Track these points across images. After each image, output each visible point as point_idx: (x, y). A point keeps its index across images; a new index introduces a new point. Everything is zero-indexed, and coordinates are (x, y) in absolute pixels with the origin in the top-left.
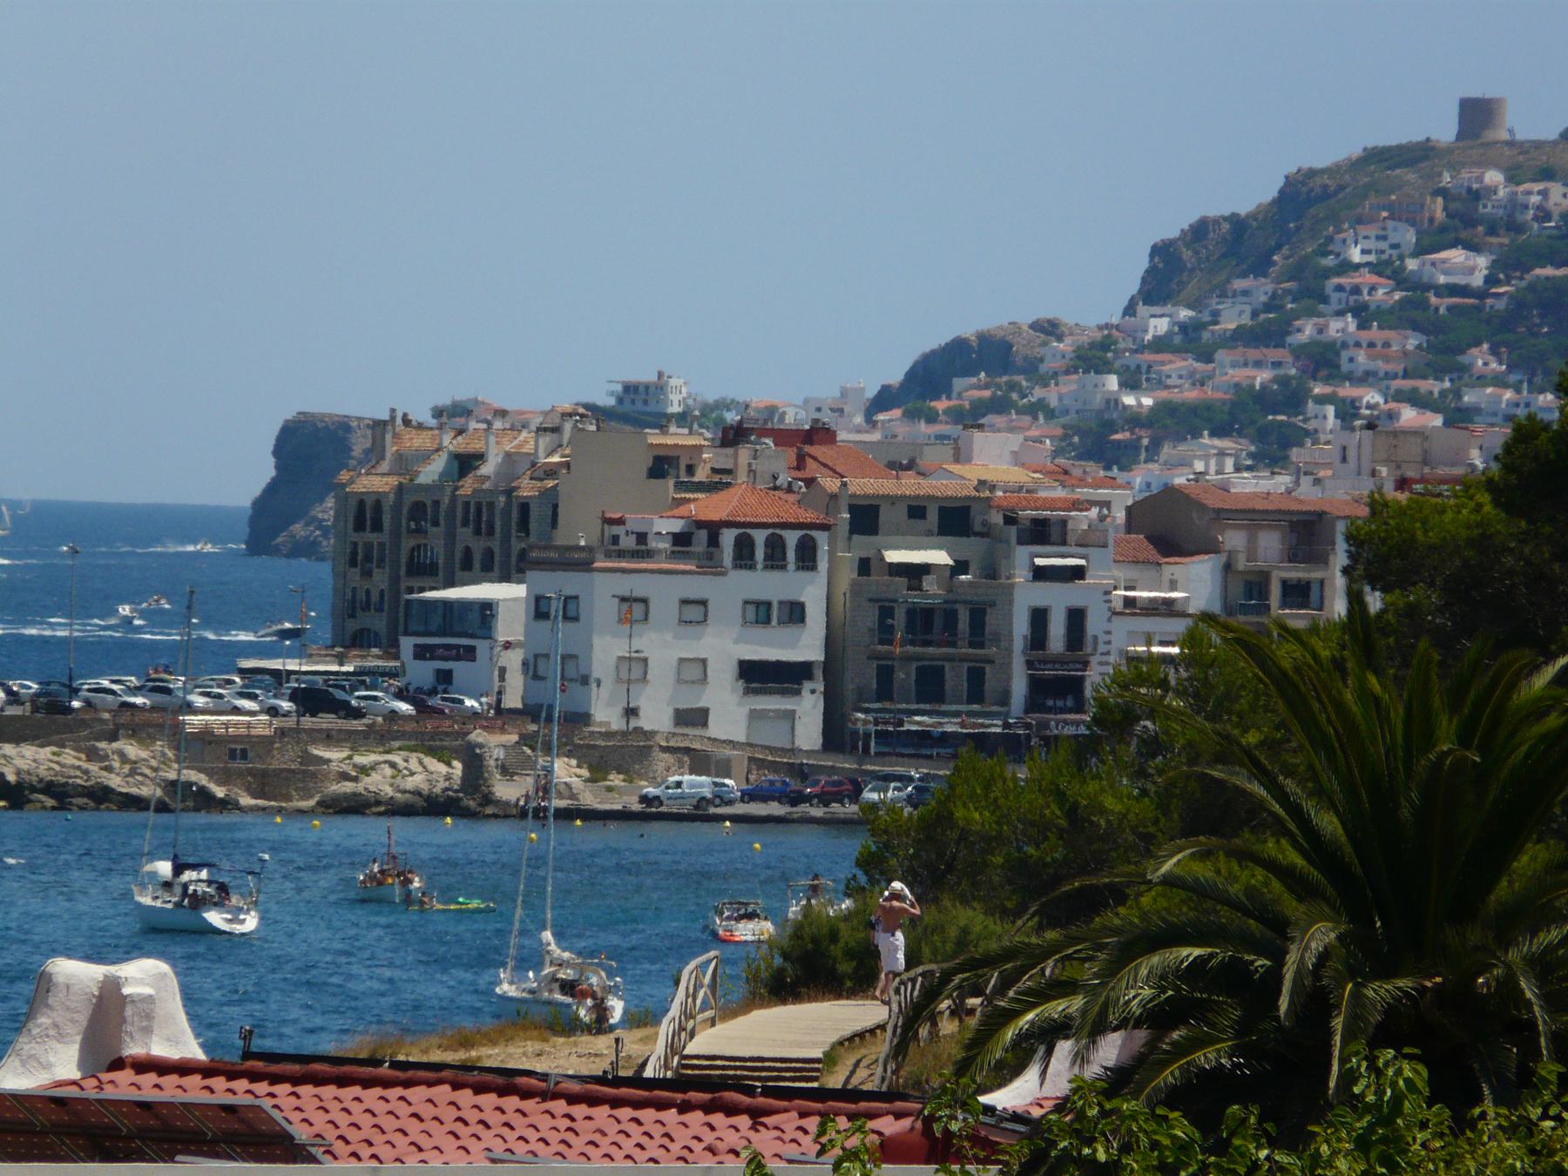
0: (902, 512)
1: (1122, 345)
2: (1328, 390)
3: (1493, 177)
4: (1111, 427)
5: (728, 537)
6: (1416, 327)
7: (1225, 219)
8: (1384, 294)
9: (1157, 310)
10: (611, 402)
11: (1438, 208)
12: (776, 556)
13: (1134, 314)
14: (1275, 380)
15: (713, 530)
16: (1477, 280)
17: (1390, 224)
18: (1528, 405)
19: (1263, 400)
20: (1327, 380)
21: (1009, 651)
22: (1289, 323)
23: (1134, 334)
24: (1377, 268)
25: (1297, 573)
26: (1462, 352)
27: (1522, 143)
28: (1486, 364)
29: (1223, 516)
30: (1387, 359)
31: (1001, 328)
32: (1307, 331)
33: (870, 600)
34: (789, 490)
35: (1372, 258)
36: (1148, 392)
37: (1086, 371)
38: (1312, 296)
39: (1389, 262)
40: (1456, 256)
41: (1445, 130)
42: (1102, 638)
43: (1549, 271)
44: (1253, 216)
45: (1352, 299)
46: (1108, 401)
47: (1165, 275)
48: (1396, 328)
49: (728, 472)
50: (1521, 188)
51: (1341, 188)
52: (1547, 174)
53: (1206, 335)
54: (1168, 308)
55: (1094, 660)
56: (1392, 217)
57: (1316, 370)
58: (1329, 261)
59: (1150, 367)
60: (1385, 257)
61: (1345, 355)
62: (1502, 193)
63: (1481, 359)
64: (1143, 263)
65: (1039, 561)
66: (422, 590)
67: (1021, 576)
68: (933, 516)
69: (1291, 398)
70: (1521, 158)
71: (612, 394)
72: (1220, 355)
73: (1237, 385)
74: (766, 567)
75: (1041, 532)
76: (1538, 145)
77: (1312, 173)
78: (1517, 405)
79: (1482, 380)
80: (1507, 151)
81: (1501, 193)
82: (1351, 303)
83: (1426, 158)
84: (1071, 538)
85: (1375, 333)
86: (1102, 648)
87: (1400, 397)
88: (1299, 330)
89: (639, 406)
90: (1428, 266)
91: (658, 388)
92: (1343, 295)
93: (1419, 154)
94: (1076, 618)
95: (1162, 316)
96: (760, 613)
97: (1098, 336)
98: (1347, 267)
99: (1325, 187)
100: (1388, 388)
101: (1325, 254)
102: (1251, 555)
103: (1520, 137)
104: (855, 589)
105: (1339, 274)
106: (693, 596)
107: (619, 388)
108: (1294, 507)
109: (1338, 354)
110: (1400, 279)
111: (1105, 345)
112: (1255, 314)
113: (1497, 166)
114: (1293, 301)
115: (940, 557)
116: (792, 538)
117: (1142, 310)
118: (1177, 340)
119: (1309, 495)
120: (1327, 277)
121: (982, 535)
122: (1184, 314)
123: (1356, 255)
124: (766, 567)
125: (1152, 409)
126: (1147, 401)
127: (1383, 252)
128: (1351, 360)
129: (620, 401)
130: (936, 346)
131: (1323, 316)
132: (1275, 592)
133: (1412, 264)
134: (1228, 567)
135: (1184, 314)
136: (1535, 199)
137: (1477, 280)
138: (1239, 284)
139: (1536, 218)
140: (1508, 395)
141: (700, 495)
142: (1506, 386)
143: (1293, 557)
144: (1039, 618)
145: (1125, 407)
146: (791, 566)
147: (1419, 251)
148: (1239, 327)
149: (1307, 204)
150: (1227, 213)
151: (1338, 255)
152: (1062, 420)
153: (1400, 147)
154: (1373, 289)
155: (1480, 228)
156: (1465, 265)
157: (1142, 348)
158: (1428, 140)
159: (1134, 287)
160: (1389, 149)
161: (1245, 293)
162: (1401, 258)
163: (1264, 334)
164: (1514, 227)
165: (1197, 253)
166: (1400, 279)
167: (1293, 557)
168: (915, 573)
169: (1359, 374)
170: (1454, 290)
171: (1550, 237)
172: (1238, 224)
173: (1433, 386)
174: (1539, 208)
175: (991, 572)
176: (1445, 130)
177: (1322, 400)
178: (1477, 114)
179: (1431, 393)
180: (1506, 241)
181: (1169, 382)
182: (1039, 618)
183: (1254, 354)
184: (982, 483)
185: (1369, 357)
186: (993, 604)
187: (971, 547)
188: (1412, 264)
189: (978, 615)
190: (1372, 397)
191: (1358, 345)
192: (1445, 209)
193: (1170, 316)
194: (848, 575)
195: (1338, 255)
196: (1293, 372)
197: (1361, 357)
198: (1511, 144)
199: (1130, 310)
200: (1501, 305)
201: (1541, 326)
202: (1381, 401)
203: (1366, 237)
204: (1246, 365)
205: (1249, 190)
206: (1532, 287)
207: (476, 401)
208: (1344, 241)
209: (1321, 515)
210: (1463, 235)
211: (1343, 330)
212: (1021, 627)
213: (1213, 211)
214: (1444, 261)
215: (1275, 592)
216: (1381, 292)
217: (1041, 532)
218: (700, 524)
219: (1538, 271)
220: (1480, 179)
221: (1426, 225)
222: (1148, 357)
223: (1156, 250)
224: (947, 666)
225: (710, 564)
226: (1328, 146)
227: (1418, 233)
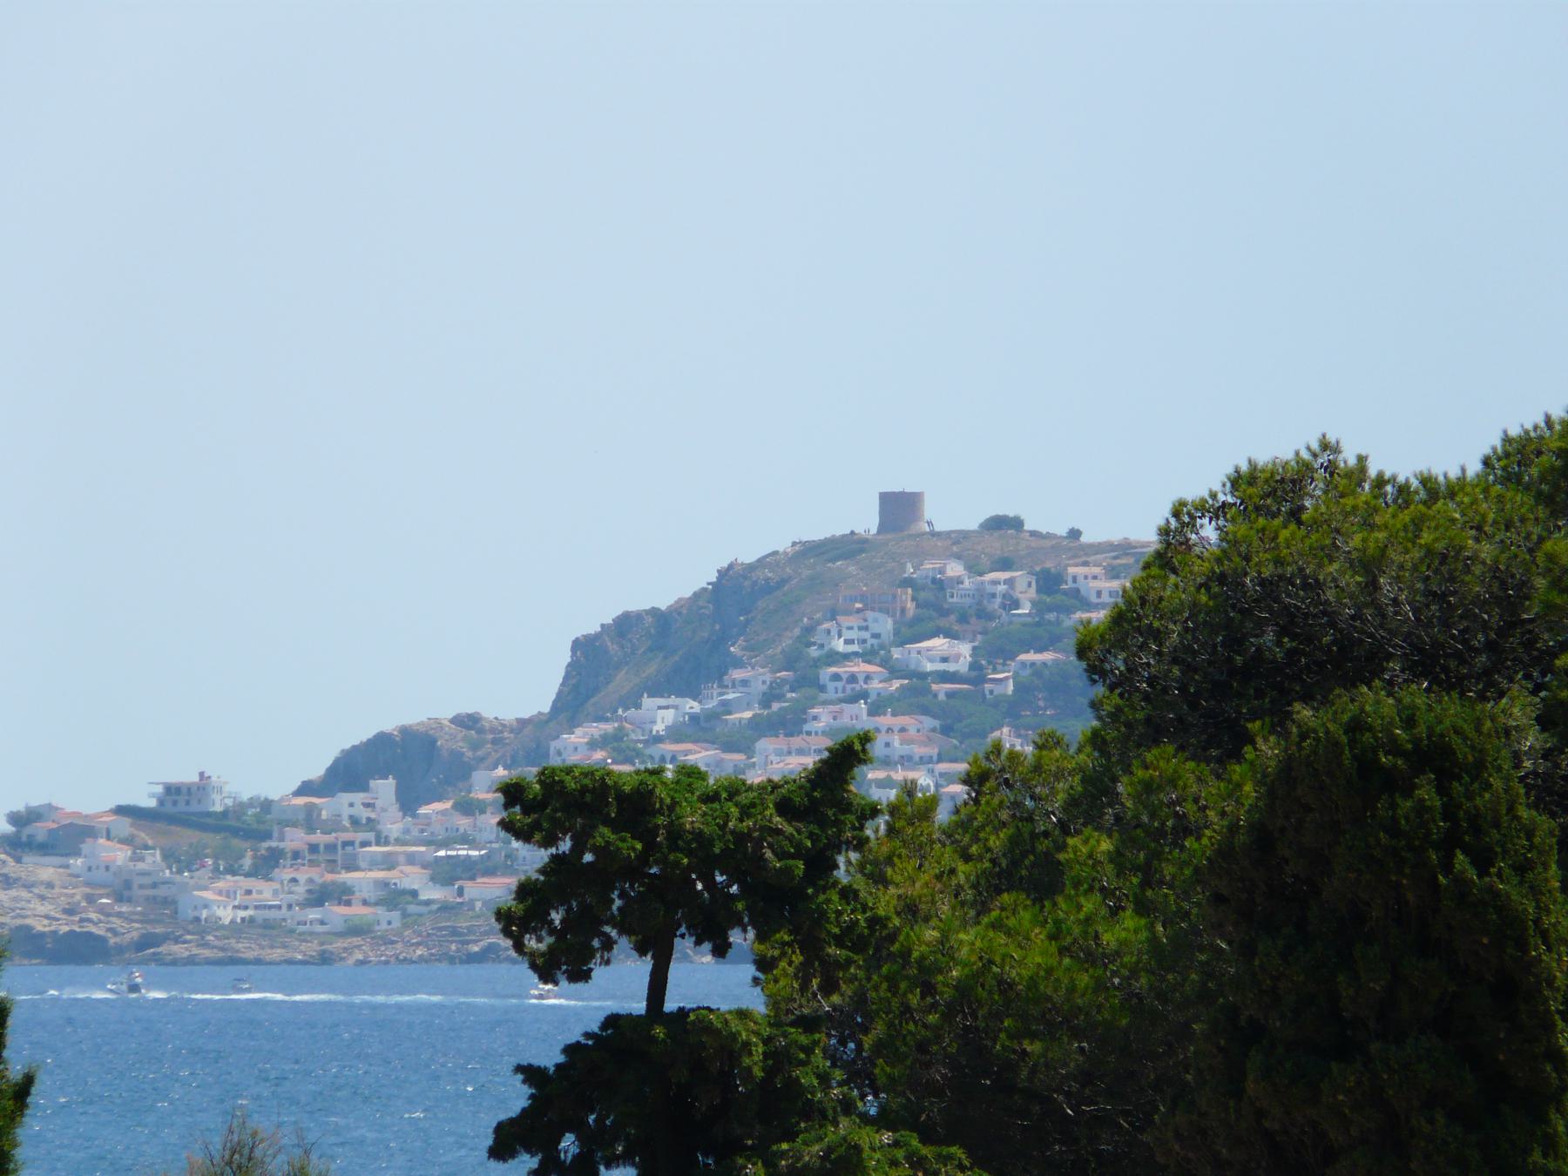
3: (955, 569)
6: (925, 711)
10: (152, 803)
11: (907, 597)
16: (962, 666)
17: (870, 615)
22: (804, 712)
24: (868, 656)
31: (422, 723)
35: (855, 648)
40: (939, 643)
41: (867, 521)
44: (678, 608)
45: (849, 687)
51: (783, 582)
54: (673, 700)
60: (868, 645)
64: (566, 658)
71: (152, 795)
81: (967, 583)
82: (848, 691)
83: (862, 551)
88: (815, 718)
89: (181, 807)
90: (914, 655)
91: (202, 787)
92: (840, 685)
93: (848, 547)
95: (667, 707)
98: (834, 658)
99: (767, 580)
103: (938, 528)
107: (159, 789)
110: (894, 671)
123: (840, 646)
127: (864, 641)
128: (887, 745)
129: (161, 802)
130: (357, 743)
133: (896, 653)
136: (1002, 588)
137: (962, 666)
139: (1003, 606)
151: (822, 646)
154: (868, 678)
158: (852, 533)
161: (745, 683)
164: (984, 615)
165: (622, 647)
170: (945, 677)
171: (1024, 625)
176: (867, 521)
178: (899, 508)
188: (896, 653)
191: (889, 730)
192: (913, 599)
193: (676, 707)
195: (822, 646)
197: (896, 741)
201: (1045, 709)
203: (850, 628)
204: (789, 753)
205: (670, 579)
207: (50, 807)
208: (829, 632)
219: (1023, 657)
220: (942, 571)
223: (577, 645)
227: (895, 623)
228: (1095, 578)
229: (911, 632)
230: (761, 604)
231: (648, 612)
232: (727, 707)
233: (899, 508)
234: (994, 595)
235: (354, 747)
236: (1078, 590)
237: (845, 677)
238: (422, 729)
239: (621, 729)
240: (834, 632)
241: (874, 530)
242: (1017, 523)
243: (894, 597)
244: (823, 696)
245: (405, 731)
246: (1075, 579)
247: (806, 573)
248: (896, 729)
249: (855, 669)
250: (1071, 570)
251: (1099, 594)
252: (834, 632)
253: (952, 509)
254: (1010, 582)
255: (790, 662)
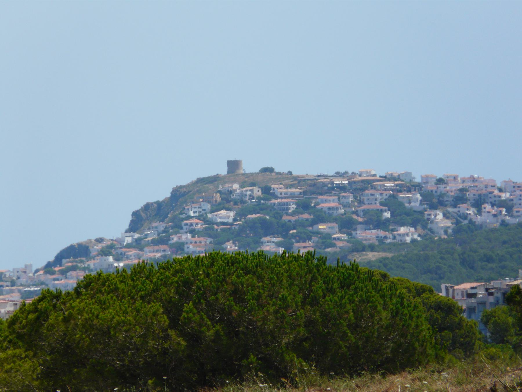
16: (231, 220)
40: (223, 212)
51: (189, 192)
64: (130, 218)
81: (238, 191)
83: (216, 181)
92: (187, 227)
95: (129, 237)
98: (189, 217)
99: (184, 192)
123: (192, 214)
127: (200, 212)
128: (188, 248)
130: (64, 248)
136: (249, 193)
139: (249, 199)
154: (197, 224)
158: (217, 175)
164: (243, 202)
171: (254, 205)
176: (223, 170)
188: (209, 216)
193: (132, 236)
197: (191, 247)
203: (195, 208)
208: (188, 209)
220: (232, 187)
228: (281, 188)
229: (216, 208)
230: (180, 200)
231: (155, 203)
232: (146, 236)
235: (68, 247)
236: (274, 193)
237: (189, 224)
238: (84, 243)
241: (226, 173)
242: (271, 170)
244: (181, 231)
245: (79, 245)
249: (192, 221)
253: (251, 166)
255: (173, 220)
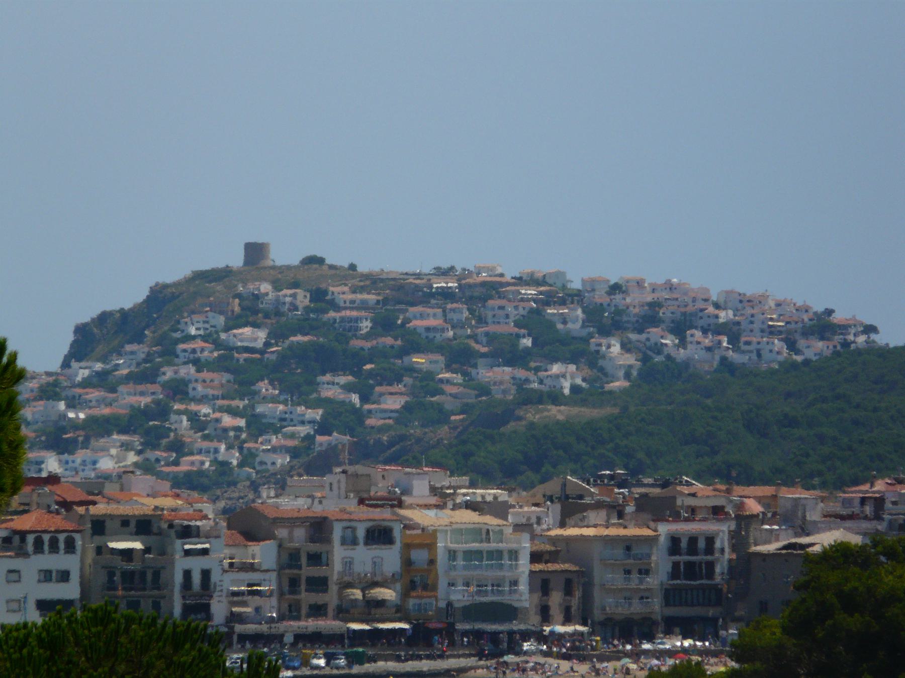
0: (118, 523)
1: (66, 384)
2: (182, 407)
3: (265, 287)
4: (64, 430)
5: (30, 539)
6: (228, 370)
7: (117, 312)
8: (209, 354)
9: (83, 364)
12: (54, 547)
13: (69, 366)
14: (153, 402)
15: (23, 535)
16: (259, 344)
17: (210, 314)
18: (291, 413)
19: (146, 413)
20: (181, 401)
21: (172, 591)
22: (158, 369)
23: (70, 378)
24: (204, 338)
25: (314, 548)
26: (254, 384)
27: (281, 267)
28: (267, 390)
29: (278, 521)
30: (213, 388)
32: (168, 373)
33: (103, 567)
34: (58, 513)
35: (201, 332)
36: (82, 409)
37: (48, 399)
38: (169, 353)
39: (210, 335)
40: (247, 331)
41: (236, 259)
42: (218, 583)
43: (299, 338)
44: (130, 310)
46: (60, 415)
47: (86, 341)
48: (217, 371)
49: (28, 504)
50: (280, 293)
52: (295, 285)
53: (110, 378)
54: (89, 364)
55: (215, 595)
56: (211, 311)
57: (175, 394)
58: (178, 335)
59: (80, 396)
60: (208, 332)
61: (191, 386)
62: (271, 296)
63: (264, 387)
64: (71, 338)
65: (187, 547)
66: (373, 659)
67: (178, 556)
68: (133, 524)
69: (161, 411)
70: (280, 276)
72: (122, 389)
73: (132, 406)
74: (50, 552)
75: (187, 533)
76: (289, 268)
77: (165, 286)
78: (286, 413)
79: (265, 400)
80: (272, 272)
81: (270, 296)
83: (226, 276)
84: (201, 534)
85: (206, 375)
86: (218, 588)
87: (221, 410)
88: (164, 374)
90: (231, 337)
92: (187, 354)
94: (206, 574)
95: (86, 368)
96: (47, 576)
97: (51, 379)
98: (190, 338)
99: (173, 293)
100: (214, 404)
101: (176, 331)
102: (291, 539)
104: (95, 562)
105: (183, 342)
106: (12, 568)
108: (311, 515)
109: (187, 386)
110: (218, 344)
111: (56, 384)
112: (138, 364)
113: (265, 280)
114: (160, 356)
115: (138, 545)
116: (62, 537)
117: (75, 365)
118: (95, 380)
119: (318, 510)
120: (177, 344)
121: (156, 534)
122: (99, 366)
123: (193, 331)
124: (50, 552)
125: (84, 420)
126: (82, 416)
127: (207, 329)
128: (194, 389)
131: (178, 365)
132: (304, 560)
133: (223, 336)
134: (280, 546)
135: (99, 366)
136: (288, 299)
137: (259, 344)
138: (128, 348)
139: (289, 310)
140: (281, 407)
141: (15, 517)
142: (280, 403)
143: (312, 540)
144: (187, 574)
145: (70, 419)
146: (62, 551)
147: (227, 329)
148: (130, 372)
149: (163, 302)
150: (118, 309)
151: (183, 331)
152: (35, 427)
153: (213, 270)
154: (202, 350)
155: (260, 315)
156: (252, 336)
157: (74, 386)
159: (65, 350)
160: (207, 271)
161: (132, 353)
162: (217, 332)
163: (145, 376)
164: (278, 313)
166: (218, 344)
167: (312, 540)
168: (127, 554)
169: (199, 397)
171: (299, 320)
172: (125, 316)
173: (241, 404)
174: (291, 304)
175: (162, 553)
176: (236, 259)
177: (179, 413)
178: (255, 252)
179: (238, 407)
180: (274, 321)
181: (91, 404)
182: (187, 574)
183: (141, 388)
184: (156, 508)
185: (204, 387)
186: (163, 568)
187: (152, 540)
188: (223, 336)
189: (157, 574)
190: (205, 410)
191: (196, 381)
192: (240, 305)
194: (91, 555)
196: (161, 396)
197: (200, 388)
198: (274, 268)
199: (66, 364)
200: (273, 357)
201: (297, 369)
202: (211, 411)
204: (135, 394)
205: (129, 295)
206: (290, 347)
208: (186, 323)
209: (325, 519)
210: (251, 319)
211: (188, 374)
212: (179, 578)
213: (109, 307)
214: (241, 334)
215: (304, 560)
216: (206, 353)
217: (187, 533)
218: (15, 532)
221: (230, 313)
222: (78, 391)
224: (142, 600)
225: (22, 553)
226: (173, 272)
228: (344, 293)
229: (235, 322)
233: (255, 252)
234: (284, 303)
239: (56, 380)
240: (189, 323)
242: (320, 261)
243: (228, 304)
246: (333, 293)
247: (192, 289)
248: (200, 380)
250: (331, 289)
251: (345, 302)
252: (189, 323)
253: (285, 254)
254: (294, 296)
